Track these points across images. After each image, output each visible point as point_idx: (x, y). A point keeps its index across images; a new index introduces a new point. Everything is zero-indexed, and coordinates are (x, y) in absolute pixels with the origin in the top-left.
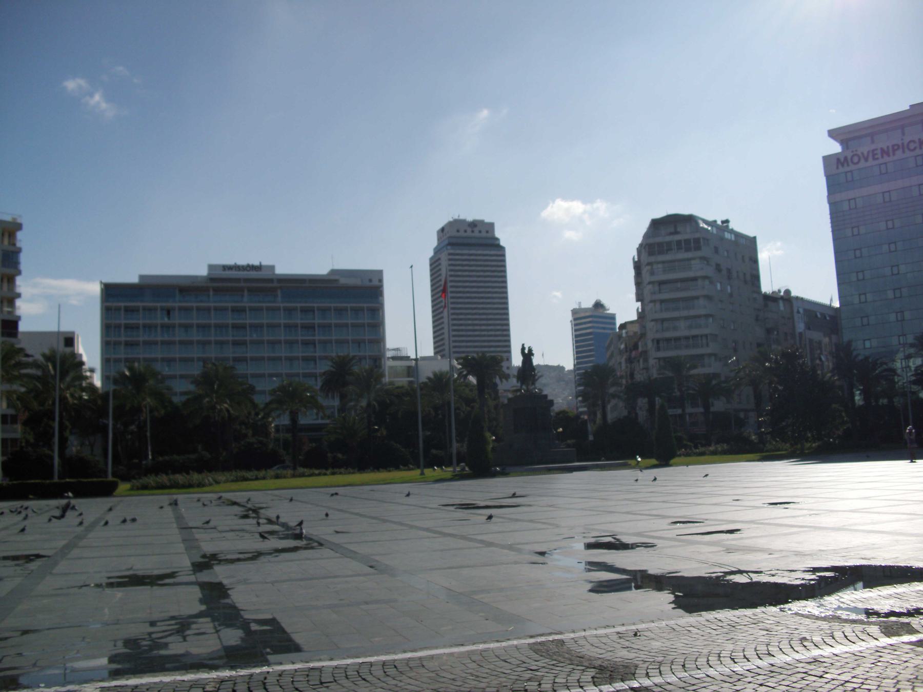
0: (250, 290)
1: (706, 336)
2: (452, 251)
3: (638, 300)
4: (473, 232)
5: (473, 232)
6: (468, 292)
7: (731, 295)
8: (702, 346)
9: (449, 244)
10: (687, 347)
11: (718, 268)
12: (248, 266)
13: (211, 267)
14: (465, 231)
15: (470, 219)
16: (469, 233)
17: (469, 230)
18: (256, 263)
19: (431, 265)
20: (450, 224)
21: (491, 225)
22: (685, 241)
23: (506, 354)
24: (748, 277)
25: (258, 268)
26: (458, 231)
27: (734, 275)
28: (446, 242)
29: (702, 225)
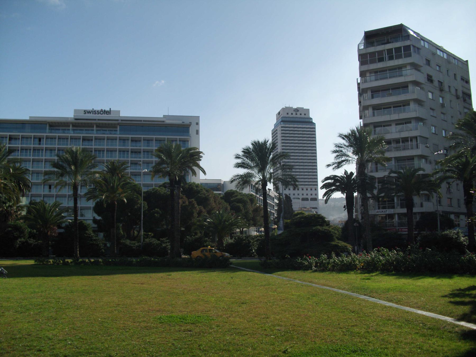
0: (98, 126)
1: (416, 137)
2: (282, 125)
3: (361, 118)
4: (296, 114)
5: (296, 114)
6: (297, 153)
7: (443, 105)
8: (412, 148)
9: (282, 121)
10: (397, 149)
11: (430, 79)
12: (102, 110)
13: (76, 111)
14: (292, 114)
15: (295, 107)
16: (294, 115)
17: (294, 113)
18: (107, 109)
19: (272, 134)
20: (283, 109)
21: (308, 110)
22: (396, 49)
23: (315, 186)
24: (460, 94)
25: (108, 112)
26: (288, 114)
27: (446, 89)
28: (281, 120)
29: (412, 33)
